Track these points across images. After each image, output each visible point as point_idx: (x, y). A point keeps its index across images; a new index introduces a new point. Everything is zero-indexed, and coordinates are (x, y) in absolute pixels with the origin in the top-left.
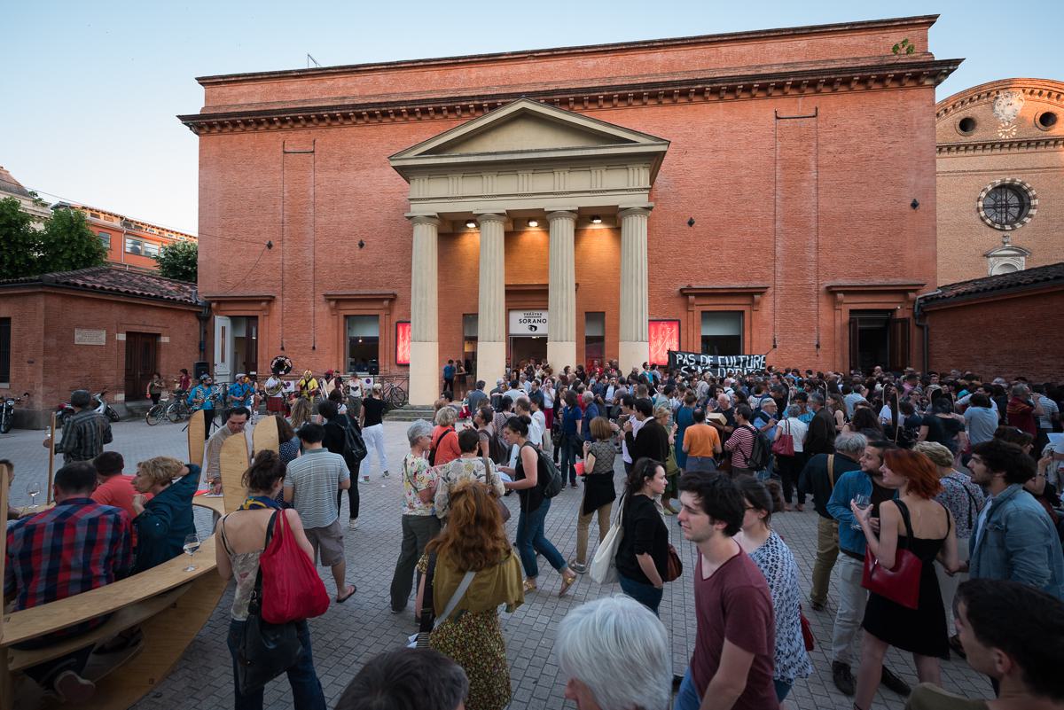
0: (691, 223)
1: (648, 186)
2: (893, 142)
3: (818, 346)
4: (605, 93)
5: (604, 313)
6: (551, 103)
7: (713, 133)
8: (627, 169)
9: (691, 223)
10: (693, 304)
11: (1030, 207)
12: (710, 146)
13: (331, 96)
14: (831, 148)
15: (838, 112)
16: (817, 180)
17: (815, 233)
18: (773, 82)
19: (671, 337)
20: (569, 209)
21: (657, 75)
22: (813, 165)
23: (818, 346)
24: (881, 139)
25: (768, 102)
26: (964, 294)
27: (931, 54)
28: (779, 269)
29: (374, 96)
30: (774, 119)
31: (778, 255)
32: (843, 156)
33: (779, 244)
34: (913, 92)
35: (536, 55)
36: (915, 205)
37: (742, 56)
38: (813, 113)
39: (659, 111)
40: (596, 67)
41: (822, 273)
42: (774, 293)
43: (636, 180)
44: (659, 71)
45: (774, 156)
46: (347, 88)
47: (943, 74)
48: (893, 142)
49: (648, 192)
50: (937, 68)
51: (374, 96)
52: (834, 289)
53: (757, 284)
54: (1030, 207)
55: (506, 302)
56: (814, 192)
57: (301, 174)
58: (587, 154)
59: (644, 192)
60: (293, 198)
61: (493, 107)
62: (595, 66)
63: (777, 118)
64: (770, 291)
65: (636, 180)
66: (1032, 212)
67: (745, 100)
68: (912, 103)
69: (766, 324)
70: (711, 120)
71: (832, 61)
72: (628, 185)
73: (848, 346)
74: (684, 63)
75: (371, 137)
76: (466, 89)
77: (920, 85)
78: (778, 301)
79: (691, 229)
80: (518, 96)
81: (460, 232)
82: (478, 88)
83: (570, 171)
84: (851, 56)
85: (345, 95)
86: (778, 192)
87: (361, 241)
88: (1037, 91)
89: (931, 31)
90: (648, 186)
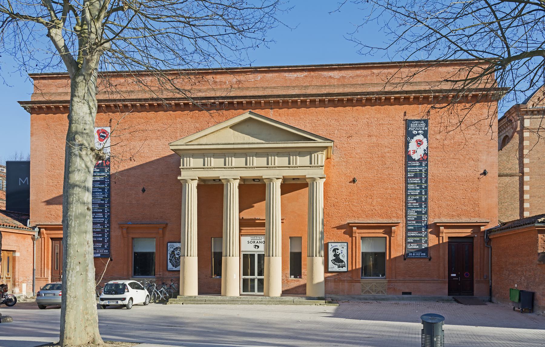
0: (354, 181)
44: (336, 84)
53: (395, 220)
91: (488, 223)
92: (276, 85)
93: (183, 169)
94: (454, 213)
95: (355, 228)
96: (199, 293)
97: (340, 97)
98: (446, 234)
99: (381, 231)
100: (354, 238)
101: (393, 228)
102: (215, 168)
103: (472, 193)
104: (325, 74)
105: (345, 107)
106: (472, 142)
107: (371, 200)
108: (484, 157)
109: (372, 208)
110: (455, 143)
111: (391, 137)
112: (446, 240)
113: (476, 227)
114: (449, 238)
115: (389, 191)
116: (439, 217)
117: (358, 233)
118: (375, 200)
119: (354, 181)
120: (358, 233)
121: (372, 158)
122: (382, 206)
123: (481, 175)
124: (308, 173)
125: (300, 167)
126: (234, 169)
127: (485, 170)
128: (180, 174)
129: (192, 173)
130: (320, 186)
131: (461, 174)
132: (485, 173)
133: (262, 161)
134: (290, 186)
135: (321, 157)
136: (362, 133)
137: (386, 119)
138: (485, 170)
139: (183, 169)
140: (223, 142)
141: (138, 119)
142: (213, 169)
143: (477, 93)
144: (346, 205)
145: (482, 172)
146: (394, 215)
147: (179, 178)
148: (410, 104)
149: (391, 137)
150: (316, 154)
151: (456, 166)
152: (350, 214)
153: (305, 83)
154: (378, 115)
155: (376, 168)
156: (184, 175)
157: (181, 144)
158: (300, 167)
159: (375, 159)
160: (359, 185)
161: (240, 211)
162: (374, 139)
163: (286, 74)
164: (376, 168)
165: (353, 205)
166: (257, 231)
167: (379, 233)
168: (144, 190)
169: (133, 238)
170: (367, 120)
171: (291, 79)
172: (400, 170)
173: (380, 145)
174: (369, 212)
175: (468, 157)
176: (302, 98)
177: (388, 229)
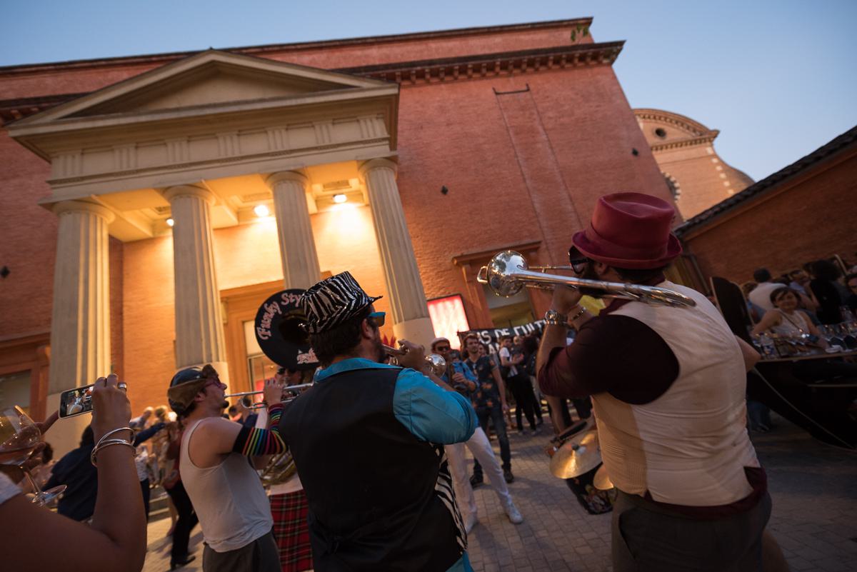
0: (444, 191)
1: (386, 135)
2: (597, 106)
7: (442, 110)
8: (358, 121)
9: (444, 191)
11: (676, 189)
14: (551, 114)
16: (549, 140)
17: (563, 187)
18: (484, 63)
19: (456, 315)
20: (292, 168)
22: (540, 129)
25: (485, 82)
28: (544, 224)
30: (494, 95)
31: (538, 211)
32: (562, 120)
33: (535, 200)
34: (596, 70)
35: (245, 51)
36: (635, 153)
38: (525, 88)
42: (547, 249)
43: (371, 131)
45: (504, 124)
47: (614, 53)
48: (597, 106)
49: (387, 142)
54: (676, 189)
56: (550, 151)
59: (384, 143)
63: (497, 94)
64: (543, 246)
65: (371, 131)
66: (678, 191)
67: (463, 81)
68: (599, 77)
70: (438, 99)
72: (362, 137)
74: (399, 56)
77: (600, 63)
78: (553, 255)
79: (446, 197)
81: (162, 235)
83: (287, 129)
86: (519, 154)
88: (647, 116)
90: (386, 135)
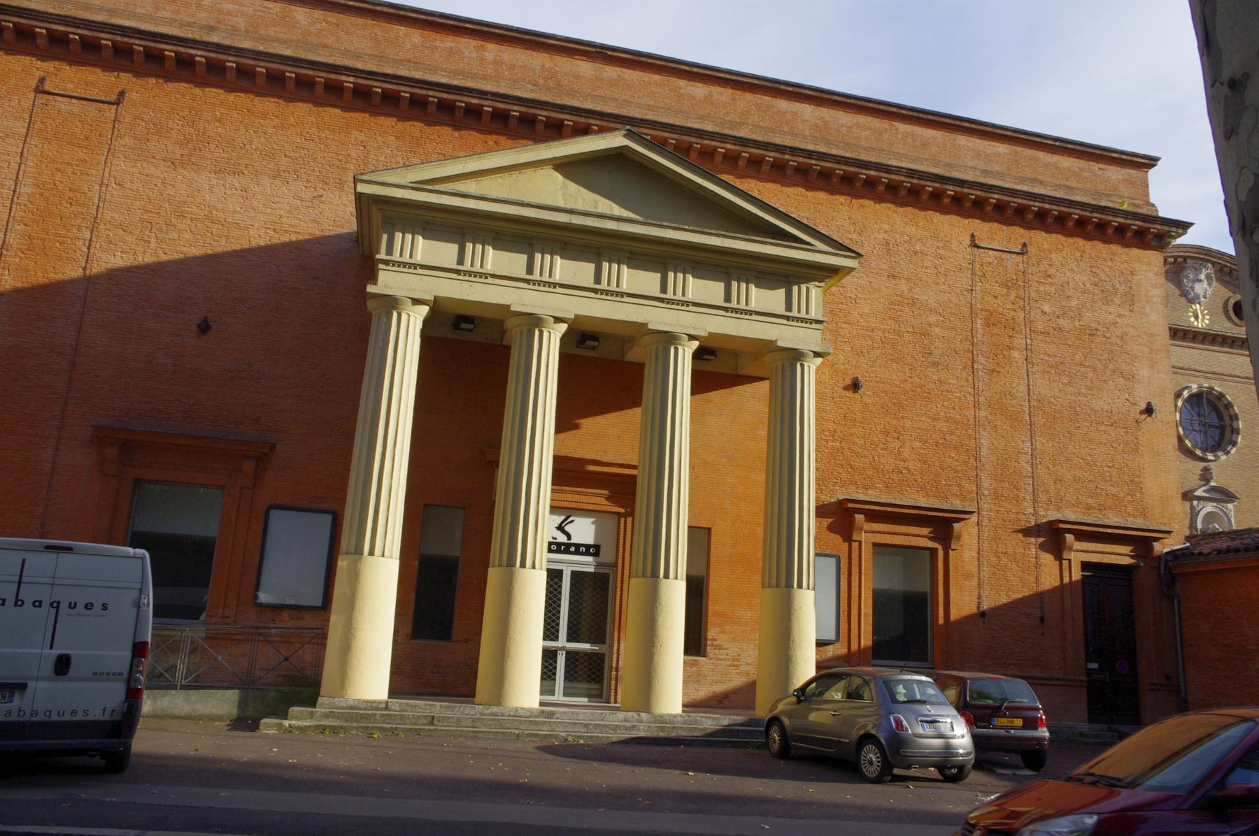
0: (855, 386)
2: (1120, 316)
3: (1042, 619)
4: (729, 146)
5: (709, 529)
6: (681, 153)
10: (1071, 549)
12: (885, 267)
13: (179, 17)
14: (1047, 308)
15: (1053, 256)
21: (805, 137)
23: (1042, 619)
24: (1105, 307)
26: (1228, 551)
27: (1153, 205)
29: (278, 40)
37: (925, 145)
39: (986, 229)
40: (708, 100)
41: (1042, 497)
44: (807, 133)
46: (220, 11)
50: (1166, 228)
51: (278, 40)
52: (850, 505)
53: (956, 504)
55: (553, 491)
57: (81, 155)
58: (406, 197)
60: (47, 200)
61: (584, 131)
62: (706, 97)
69: (968, 576)
71: (1041, 183)
73: (1081, 621)
75: (265, 116)
76: (1034, 181)
80: (609, 121)
82: (190, 24)
84: (1063, 182)
85: (212, 23)
87: (205, 320)
89: (1152, 173)
91: (1169, 532)
92: (652, 103)
93: (387, 262)
94: (1090, 501)
95: (859, 518)
96: (394, 692)
97: (828, 165)
98: (1080, 553)
99: (925, 531)
100: (855, 545)
101: (956, 525)
102: (494, 280)
103: (1126, 456)
104: (783, 104)
105: (832, 193)
106: (1119, 332)
107: (896, 444)
108: (1143, 372)
109: (901, 464)
110: (1083, 329)
111: (942, 287)
112: (1077, 575)
113: (1141, 543)
114: (1085, 566)
115: (941, 425)
116: (1059, 509)
117: (869, 534)
118: (908, 445)
119: (855, 386)
120: (869, 534)
121: (898, 333)
122: (925, 462)
123: (1141, 413)
124: (786, 336)
125: (759, 315)
126: (559, 290)
127: (1149, 404)
128: (373, 278)
129: (418, 278)
130: (810, 375)
131: (1099, 404)
132: (1149, 410)
133: (648, 281)
134: (719, 367)
135: (813, 297)
136: (873, 264)
137: (930, 242)
138: (1149, 404)
139: (387, 262)
140: (539, 201)
141: (220, 108)
142: (490, 280)
143: (1128, 222)
144: (833, 447)
145: (1143, 406)
146: (955, 489)
147: (371, 289)
148: (985, 218)
149: (942, 287)
150: (803, 287)
151: (1089, 383)
152: (844, 476)
153: (728, 113)
154: (911, 230)
155: (909, 359)
156: (387, 282)
157: (398, 183)
158: (759, 315)
159: (907, 337)
160: (868, 400)
161: (564, 424)
162: (903, 286)
163: (682, 83)
164: (909, 359)
165: (853, 451)
166: (576, 498)
167: (919, 537)
168: (204, 327)
169: (138, 482)
170: (886, 236)
171: (693, 98)
172: (964, 374)
173: (918, 305)
174: (894, 476)
175: (1111, 367)
176: (729, 146)
177: (943, 526)
